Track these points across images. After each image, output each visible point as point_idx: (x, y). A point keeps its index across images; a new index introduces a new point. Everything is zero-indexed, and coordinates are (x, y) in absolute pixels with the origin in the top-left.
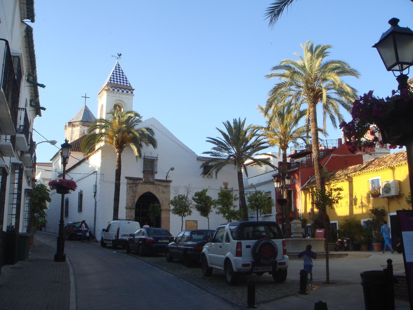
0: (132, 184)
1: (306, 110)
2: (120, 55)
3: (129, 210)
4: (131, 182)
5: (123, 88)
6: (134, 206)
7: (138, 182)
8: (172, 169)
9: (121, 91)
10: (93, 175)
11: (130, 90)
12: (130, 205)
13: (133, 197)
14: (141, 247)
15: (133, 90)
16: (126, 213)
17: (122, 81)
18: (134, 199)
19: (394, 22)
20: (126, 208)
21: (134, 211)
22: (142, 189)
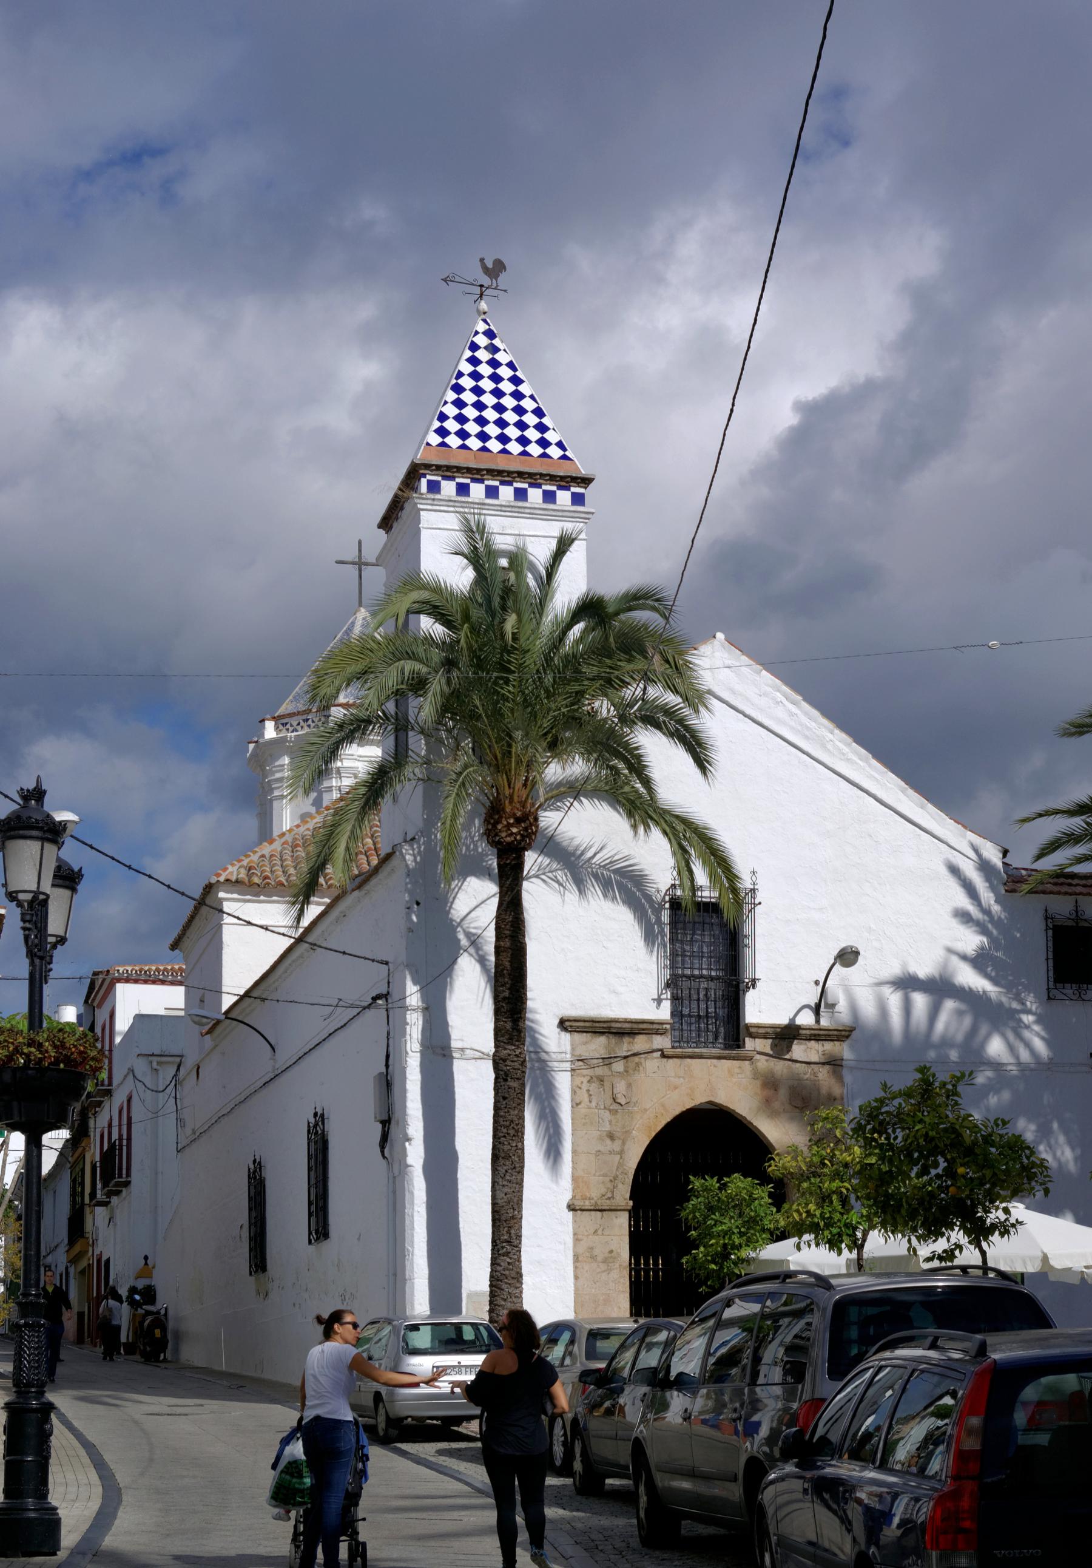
0: (608, 1061)
1: (624, 1417)
2: (445, 280)
3: (591, 1220)
4: (598, 1046)
5: (521, 475)
6: (623, 1192)
7: (640, 1043)
8: (847, 957)
9: (506, 493)
10: (369, 1014)
11: (565, 482)
12: (595, 1192)
13: (611, 1137)
14: (961, 1170)
15: (586, 481)
16: (577, 1239)
17: (492, 430)
18: (621, 1153)
19: (319, 1319)
20: (571, 1208)
21: (622, 1223)
22: (674, 1086)
